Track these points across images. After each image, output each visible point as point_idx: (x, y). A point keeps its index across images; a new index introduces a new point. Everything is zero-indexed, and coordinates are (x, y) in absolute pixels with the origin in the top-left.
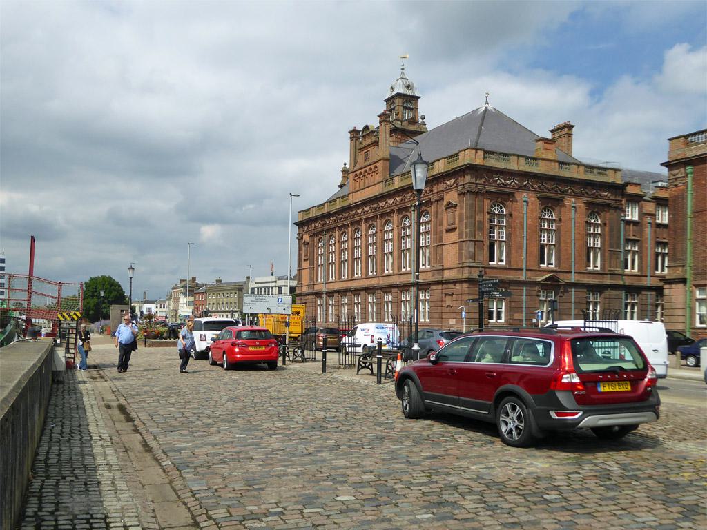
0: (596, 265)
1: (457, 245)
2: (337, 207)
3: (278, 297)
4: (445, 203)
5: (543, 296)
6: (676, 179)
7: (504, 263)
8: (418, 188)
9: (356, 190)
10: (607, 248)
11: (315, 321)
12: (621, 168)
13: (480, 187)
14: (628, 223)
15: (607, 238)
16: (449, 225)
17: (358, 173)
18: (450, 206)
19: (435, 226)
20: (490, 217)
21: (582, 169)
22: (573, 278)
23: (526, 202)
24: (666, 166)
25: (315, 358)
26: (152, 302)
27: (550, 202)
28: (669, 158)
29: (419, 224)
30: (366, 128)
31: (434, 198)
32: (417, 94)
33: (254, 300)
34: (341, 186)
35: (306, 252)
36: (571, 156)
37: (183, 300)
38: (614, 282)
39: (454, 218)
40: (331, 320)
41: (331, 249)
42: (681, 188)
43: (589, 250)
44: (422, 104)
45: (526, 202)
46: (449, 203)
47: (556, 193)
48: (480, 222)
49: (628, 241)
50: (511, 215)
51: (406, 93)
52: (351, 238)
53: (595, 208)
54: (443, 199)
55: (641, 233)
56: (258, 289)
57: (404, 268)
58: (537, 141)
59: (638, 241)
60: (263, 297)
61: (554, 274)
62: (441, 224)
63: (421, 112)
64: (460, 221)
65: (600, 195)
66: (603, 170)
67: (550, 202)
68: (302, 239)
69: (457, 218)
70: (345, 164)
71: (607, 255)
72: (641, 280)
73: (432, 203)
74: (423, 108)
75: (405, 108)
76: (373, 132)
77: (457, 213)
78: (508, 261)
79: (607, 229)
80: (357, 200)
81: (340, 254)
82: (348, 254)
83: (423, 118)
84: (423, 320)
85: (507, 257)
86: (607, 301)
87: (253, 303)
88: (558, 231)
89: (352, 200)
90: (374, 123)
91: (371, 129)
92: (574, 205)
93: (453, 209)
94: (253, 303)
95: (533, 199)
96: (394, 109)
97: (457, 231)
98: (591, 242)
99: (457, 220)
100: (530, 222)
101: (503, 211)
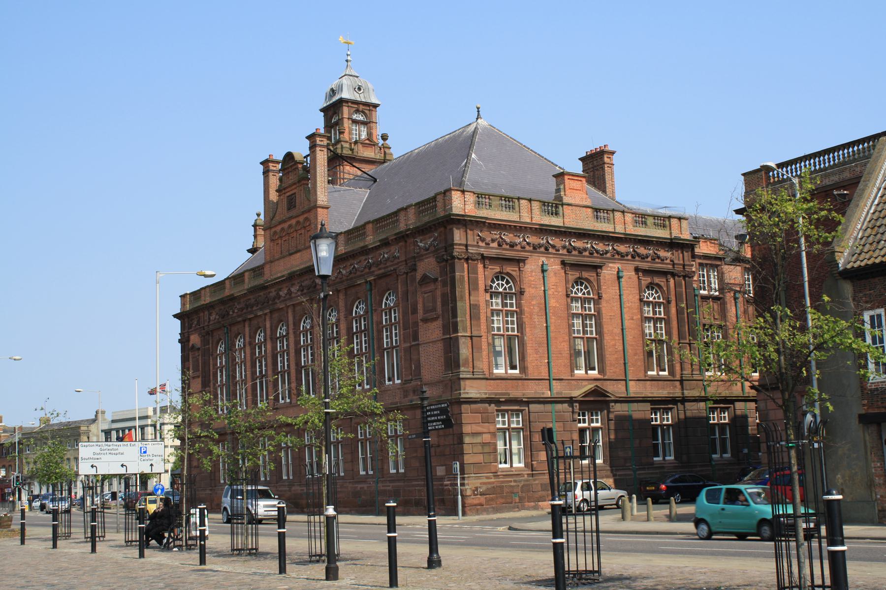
1: (440, 345)
2: (246, 287)
3: (139, 444)
4: (419, 276)
5: (656, 419)
8: (322, 273)
9: (276, 257)
11: (603, 489)
12: (687, 215)
17: (279, 228)
19: (405, 314)
21: (629, 217)
25: (256, 549)
29: (274, 339)
30: (289, 156)
32: (374, 100)
33: (99, 451)
34: (252, 251)
35: (197, 361)
36: (613, 199)
39: (434, 301)
44: (379, 115)
51: (353, 98)
52: (271, 339)
53: (651, 275)
56: (117, 431)
57: (389, 380)
60: (114, 444)
61: (598, 383)
62: (415, 311)
63: (378, 131)
64: (443, 305)
66: (663, 220)
68: (188, 341)
69: (439, 300)
70: (258, 215)
74: (383, 123)
77: (439, 293)
80: (279, 275)
81: (253, 366)
82: (266, 365)
83: (384, 137)
84: (395, 471)
87: (97, 457)
89: (269, 275)
90: (301, 150)
93: (432, 287)
94: (97, 457)
99: (439, 304)
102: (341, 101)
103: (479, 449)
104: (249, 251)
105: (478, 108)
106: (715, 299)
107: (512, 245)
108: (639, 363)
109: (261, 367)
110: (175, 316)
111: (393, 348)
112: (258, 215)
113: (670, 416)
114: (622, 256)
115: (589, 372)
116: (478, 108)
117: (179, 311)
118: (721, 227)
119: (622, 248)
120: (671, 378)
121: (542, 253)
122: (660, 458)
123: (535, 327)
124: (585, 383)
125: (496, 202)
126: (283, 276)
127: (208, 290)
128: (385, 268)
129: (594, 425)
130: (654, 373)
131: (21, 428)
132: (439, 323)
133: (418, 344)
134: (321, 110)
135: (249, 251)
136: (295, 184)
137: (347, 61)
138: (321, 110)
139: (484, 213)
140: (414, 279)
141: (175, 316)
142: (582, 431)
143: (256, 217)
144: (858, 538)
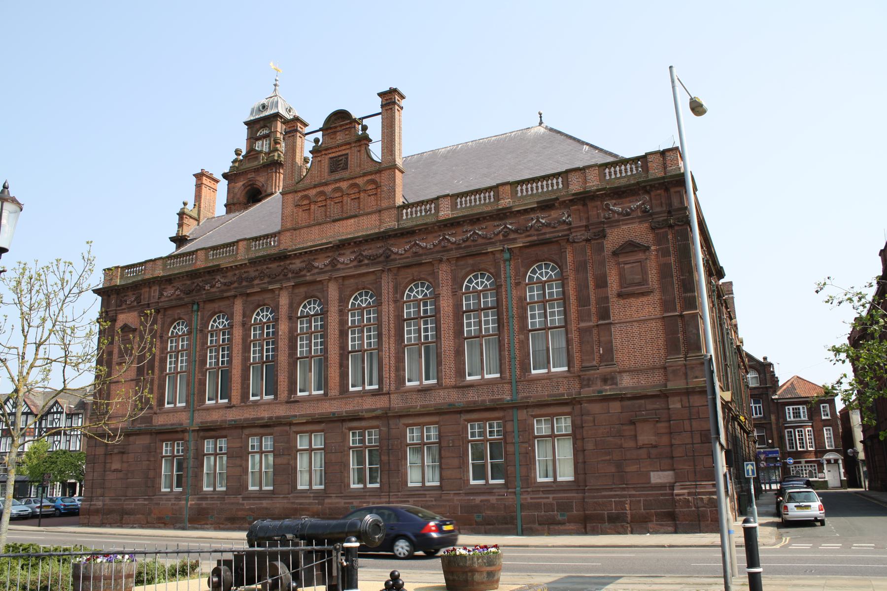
89: (288, 243)
102: (277, 116)
104: (172, 239)
105: (540, 114)
111: (178, 373)
112: (185, 204)
116: (540, 114)
117: (101, 286)
126: (330, 243)
127: (159, 263)
128: (538, 235)
131: (733, 298)
132: (656, 297)
133: (611, 323)
134: (246, 123)
135: (172, 239)
136: (349, 144)
137: (275, 85)
138: (246, 123)
140: (601, 248)
141: (97, 291)
143: (183, 206)
144: (691, 546)
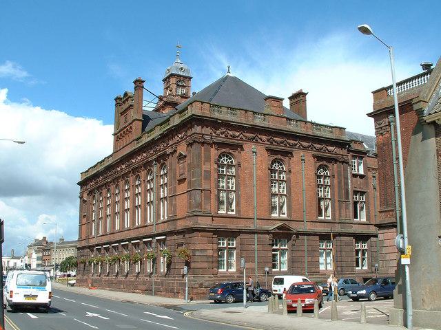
0: (328, 215)
4: (177, 154)
6: (381, 128)
7: (234, 213)
10: (337, 198)
13: (208, 138)
14: (355, 176)
15: (336, 189)
16: (180, 175)
18: (182, 157)
20: (219, 167)
22: (308, 227)
23: (254, 156)
24: (372, 116)
26: (18, 258)
27: (279, 155)
28: (374, 109)
30: (126, 94)
31: (169, 151)
37: (35, 256)
38: (344, 231)
40: (149, 271)
41: (101, 204)
42: (386, 136)
43: (320, 200)
45: (254, 156)
46: (181, 154)
47: (285, 146)
48: (206, 171)
49: (355, 193)
50: (239, 166)
53: (324, 161)
54: (176, 151)
55: (367, 184)
58: (266, 100)
59: (365, 192)
61: (286, 223)
65: (328, 150)
67: (279, 155)
71: (337, 204)
72: (369, 228)
73: (168, 155)
75: (178, 86)
76: (130, 97)
78: (238, 211)
79: (336, 181)
85: (237, 205)
86: (339, 249)
88: (288, 181)
91: (129, 95)
92: (302, 163)
95: (261, 150)
96: (169, 87)
97: (186, 182)
98: (321, 194)
100: (259, 173)
101: (232, 162)
103: (205, 259)
106: (362, 177)
107: (234, 137)
108: (313, 211)
109: (150, 196)
110: (369, 115)
113: (235, 242)
114: (305, 148)
115: (281, 215)
117: (372, 111)
118: (370, 138)
119: (305, 144)
120: (368, 222)
121: (254, 142)
122: (360, 268)
123: (246, 187)
124: (279, 222)
125: (224, 110)
129: (283, 247)
130: (323, 218)
139: (216, 115)
141: (369, 115)
142: (357, 251)
